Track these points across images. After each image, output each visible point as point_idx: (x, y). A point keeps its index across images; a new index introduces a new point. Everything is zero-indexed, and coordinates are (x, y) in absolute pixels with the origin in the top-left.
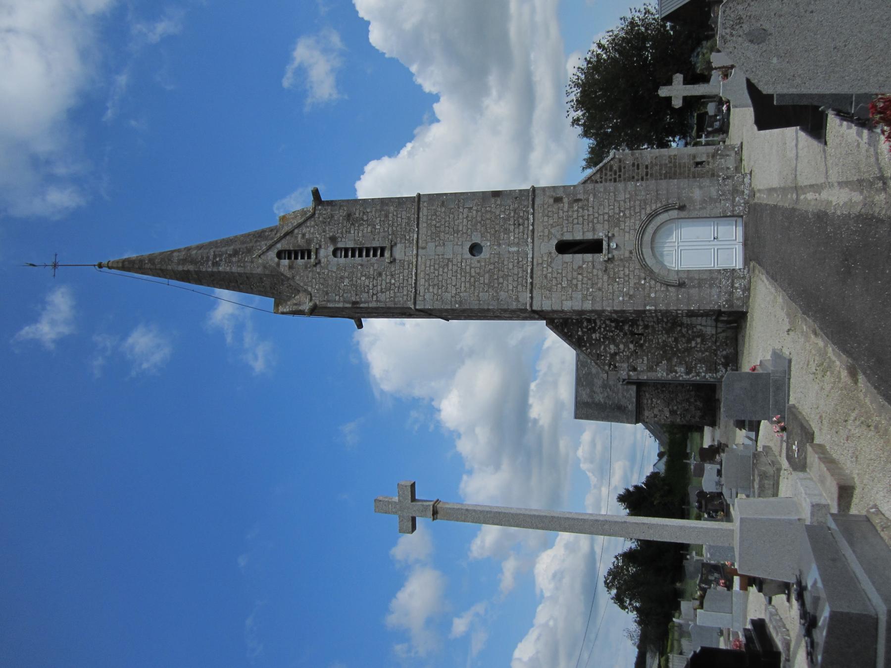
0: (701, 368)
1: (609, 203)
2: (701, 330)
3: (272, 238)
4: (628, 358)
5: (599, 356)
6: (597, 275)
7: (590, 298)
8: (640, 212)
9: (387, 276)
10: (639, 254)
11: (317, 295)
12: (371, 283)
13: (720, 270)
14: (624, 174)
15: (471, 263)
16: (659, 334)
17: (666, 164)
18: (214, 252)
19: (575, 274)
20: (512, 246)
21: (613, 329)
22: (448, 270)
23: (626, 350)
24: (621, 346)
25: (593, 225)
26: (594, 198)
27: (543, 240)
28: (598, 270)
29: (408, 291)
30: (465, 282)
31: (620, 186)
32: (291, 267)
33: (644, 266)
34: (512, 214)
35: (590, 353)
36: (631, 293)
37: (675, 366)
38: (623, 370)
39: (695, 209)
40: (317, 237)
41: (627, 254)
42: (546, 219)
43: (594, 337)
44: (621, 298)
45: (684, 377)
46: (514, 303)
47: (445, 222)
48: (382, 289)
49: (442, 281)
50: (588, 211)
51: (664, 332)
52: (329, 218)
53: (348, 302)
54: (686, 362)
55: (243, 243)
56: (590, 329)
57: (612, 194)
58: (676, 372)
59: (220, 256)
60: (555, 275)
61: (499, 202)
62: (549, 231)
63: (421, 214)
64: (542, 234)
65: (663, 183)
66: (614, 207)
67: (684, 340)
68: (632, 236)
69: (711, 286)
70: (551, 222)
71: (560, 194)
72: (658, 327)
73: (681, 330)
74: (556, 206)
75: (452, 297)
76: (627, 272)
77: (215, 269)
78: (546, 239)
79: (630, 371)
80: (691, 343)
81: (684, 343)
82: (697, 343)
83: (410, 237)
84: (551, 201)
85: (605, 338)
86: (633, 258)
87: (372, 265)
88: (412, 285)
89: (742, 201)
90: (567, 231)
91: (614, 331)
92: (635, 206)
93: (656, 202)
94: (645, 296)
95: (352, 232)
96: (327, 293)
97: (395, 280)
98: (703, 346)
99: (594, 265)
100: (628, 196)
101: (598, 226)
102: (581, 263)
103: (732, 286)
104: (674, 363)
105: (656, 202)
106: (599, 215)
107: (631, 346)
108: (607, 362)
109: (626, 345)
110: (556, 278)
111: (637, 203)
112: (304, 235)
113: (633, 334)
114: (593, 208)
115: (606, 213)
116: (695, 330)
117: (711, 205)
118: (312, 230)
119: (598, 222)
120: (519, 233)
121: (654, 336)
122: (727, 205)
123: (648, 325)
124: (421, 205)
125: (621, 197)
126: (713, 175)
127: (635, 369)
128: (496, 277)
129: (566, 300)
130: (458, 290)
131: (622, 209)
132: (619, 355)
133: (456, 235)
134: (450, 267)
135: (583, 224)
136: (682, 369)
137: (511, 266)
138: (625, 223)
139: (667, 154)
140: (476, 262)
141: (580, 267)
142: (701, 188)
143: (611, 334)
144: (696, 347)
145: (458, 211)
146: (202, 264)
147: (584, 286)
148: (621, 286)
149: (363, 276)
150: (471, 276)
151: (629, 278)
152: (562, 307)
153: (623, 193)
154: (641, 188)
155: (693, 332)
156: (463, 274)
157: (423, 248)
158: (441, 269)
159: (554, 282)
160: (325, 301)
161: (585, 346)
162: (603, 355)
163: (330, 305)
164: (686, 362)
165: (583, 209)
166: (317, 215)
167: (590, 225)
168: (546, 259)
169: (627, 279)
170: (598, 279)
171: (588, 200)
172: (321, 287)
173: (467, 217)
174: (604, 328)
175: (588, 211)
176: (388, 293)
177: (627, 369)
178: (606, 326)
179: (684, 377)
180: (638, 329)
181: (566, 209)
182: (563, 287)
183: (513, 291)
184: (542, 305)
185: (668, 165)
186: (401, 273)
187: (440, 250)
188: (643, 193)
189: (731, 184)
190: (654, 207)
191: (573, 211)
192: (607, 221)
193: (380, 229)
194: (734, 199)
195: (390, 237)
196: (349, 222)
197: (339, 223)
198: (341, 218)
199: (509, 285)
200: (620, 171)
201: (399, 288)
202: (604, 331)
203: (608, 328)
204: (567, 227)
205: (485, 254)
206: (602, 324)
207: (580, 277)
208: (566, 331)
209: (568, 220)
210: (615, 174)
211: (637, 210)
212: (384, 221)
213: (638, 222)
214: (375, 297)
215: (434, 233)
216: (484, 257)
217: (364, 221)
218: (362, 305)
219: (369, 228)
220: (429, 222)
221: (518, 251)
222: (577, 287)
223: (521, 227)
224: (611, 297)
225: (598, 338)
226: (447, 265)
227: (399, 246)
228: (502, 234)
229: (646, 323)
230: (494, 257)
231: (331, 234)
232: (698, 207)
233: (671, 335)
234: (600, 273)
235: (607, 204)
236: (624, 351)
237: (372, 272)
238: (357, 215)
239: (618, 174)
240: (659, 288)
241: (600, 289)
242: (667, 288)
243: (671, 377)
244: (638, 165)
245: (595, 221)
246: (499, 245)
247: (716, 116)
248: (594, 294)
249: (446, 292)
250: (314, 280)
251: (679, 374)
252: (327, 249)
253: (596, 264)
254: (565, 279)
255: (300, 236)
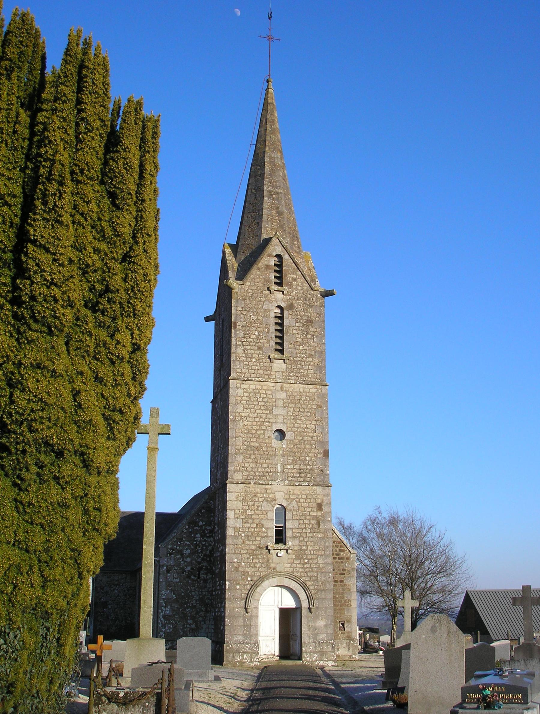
0: (169, 628)
1: (316, 550)
2: (203, 628)
3: (292, 248)
4: (179, 565)
5: (181, 540)
6: (256, 540)
7: (237, 534)
8: (307, 576)
9: (259, 354)
10: (297, 580)
11: (242, 290)
12: (252, 340)
13: (258, 642)
14: (337, 562)
15: (268, 431)
16: (199, 592)
17: (344, 598)
18: (281, 193)
19: (258, 521)
20: (282, 467)
21: (204, 553)
22: (263, 410)
23: (186, 563)
24: (189, 560)
25: (297, 537)
26: (320, 538)
27: (286, 494)
28: (260, 541)
29: (245, 374)
30: (252, 425)
31: (330, 560)
32: (267, 267)
33: (262, 579)
34: (309, 467)
35: (183, 532)
36: (240, 569)
37: (171, 606)
38: (167, 561)
39: (308, 621)
40: (293, 292)
41: (273, 565)
42: (304, 496)
43: (197, 535)
44: (236, 560)
45: (161, 614)
46: (233, 469)
47: (304, 409)
48: (247, 350)
49: (253, 404)
50: (310, 533)
51: (201, 596)
52: (310, 304)
53: (236, 319)
54: (174, 615)
55: (289, 220)
56: (204, 532)
57: (323, 552)
58: (165, 607)
59: (277, 199)
60: (256, 504)
61: (319, 456)
62: (294, 499)
63: (311, 386)
64: (291, 493)
65: (331, 595)
66: (313, 555)
67: (193, 613)
68: (287, 569)
69: (244, 635)
70: (301, 501)
71: (325, 509)
72: (205, 592)
73: (202, 611)
74: (314, 505)
75: (239, 413)
76: (258, 565)
77: (265, 193)
78: (286, 496)
79: (167, 567)
80: (191, 619)
81: (191, 614)
82: (190, 624)
83: (292, 376)
84: (319, 501)
85: (196, 545)
86: (269, 571)
87: (268, 342)
88: (250, 377)
89: (314, 659)
90: (293, 515)
91: (202, 553)
92: (313, 572)
93: (315, 589)
94: (237, 580)
95: (297, 324)
96: (244, 300)
97: (255, 362)
98: (188, 629)
99: (264, 537)
100: (321, 566)
101: (296, 542)
102: (267, 527)
103: (244, 653)
104: (173, 605)
105: (315, 589)
106: (306, 542)
107: (189, 568)
108: (175, 547)
109: (189, 564)
110: (254, 505)
111: (315, 574)
112: (295, 280)
113: (200, 569)
114: (312, 537)
115: (307, 548)
116: (202, 623)
117: (312, 634)
118: (299, 288)
119: (300, 541)
120: (293, 473)
121: (197, 588)
122: (312, 648)
123: (208, 583)
124: (318, 387)
125: (320, 561)
126: (335, 637)
127: (168, 571)
128: (255, 453)
129: (235, 514)
130: (245, 419)
131: (310, 561)
132: (181, 558)
133: (292, 417)
134: (264, 412)
135: (299, 528)
136: (168, 612)
137: (265, 465)
138: (299, 564)
139: (352, 598)
140: (268, 435)
141: (262, 526)
142: (326, 626)
143: (200, 551)
144: (188, 624)
145: (313, 420)
146: (270, 181)
147: (247, 529)
148: (246, 561)
149: (259, 333)
150: (257, 430)
151: (252, 567)
152: (230, 510)
153: (323, 562)
154: (327, 577)
155: (200, 621)
156: (259, 423)
157: (282, 388)
158: (263, 404)
159: (250, 503)
160: (237, 297)
161: (189, 527)
162: (181, 543)
163: (234, 302)
164: (174, 615)
165: (311, 528)
166: (312, 292)
167: (298, 535)
168: (270, 496)
169: (252, 565)
170: (253, 541)
171: (319, 532)
172: (250, 295)
173: (307, 428)
174: (205, 544)
175: (310, 533)
176: (244, 355)
177: (168, 564)
178: (207, 547)
179: (161, 614)
180: (203, 574)
181: (312, 514)
182: (246, 510)
183: (243, 467)
184: (230, 492)
185: (342, 600)
186: (261, 367)
187: (280, 403)
188: (323, 579)
189: (327, 650)
190: (311, 588)
191: (310, 520)
192: (301, 548)
193: (299, 349)
194: (316, 653)
195: (292, 359)
196: (306, 322)
197: (305, 313)
198: (309, 315)
199: (248, 464)
200: (339, 559)
201: (248, 365)
202: (202, 544)
203: (204, 548)
204: (297, 515)
205: (276, 443)
206: (209, 543)
207: (255, 525)
208: (203, 511)
209: (302, 515)
210: (337, 555)
211: (309, 574)
212: (306, 353)
213: (299, 574)
214: (240, 343)
215: (294, 398)
216: (273, 442)
217: (306, 336)
218: (233, 331)
219: (299, 340)
220: (304, 394)
221: (278, 472)
222: (245, 523)
223: (298, 475)
224: (237, 552)
225: (196, 539)
226: (266, 410)
227: (284, 366)
228: (292, 458)
229: (209, 581)
230: (273, 451)
231: (295, 305)
232: (310, 624)
233: (198, 602)
234: (257, 543)
235: (315, 548)
236: (185, 561)
237: (261, 341)
238: (311, 329)
239: (337, 557)
240: (244, 592)
241: (243, 542)
242: (243, 599)
243: (162, 603)
244: (343, 574)
245: (301, 539)
246: (283, 456)
247: (379, 642)
248: (240, 537)
249: (244, 408)
250: (256, 288)
251: (164, 609)
252: (283, 301)
253: (265, 539)
254: (253, 512)
255: (295, 276)
